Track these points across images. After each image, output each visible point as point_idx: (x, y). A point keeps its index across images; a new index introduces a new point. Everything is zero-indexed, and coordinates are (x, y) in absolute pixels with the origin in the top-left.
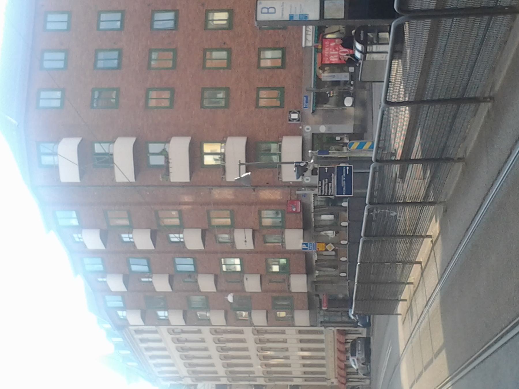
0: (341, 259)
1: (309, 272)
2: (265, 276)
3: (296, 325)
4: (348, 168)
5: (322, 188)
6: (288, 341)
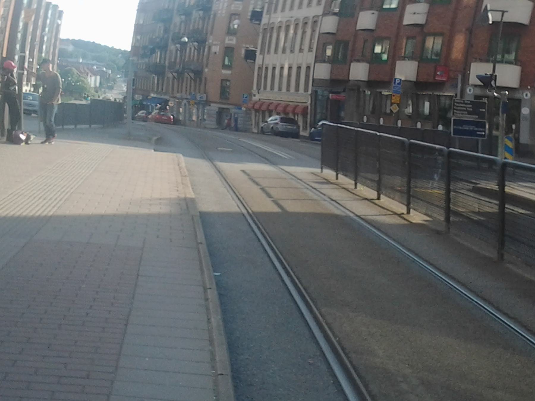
0: (382, 119)
1: (371, 84)
2: (373, 36)
3: (316, 64)
4: (483, 133)
5: (461, 103)
6: (300, 54)
